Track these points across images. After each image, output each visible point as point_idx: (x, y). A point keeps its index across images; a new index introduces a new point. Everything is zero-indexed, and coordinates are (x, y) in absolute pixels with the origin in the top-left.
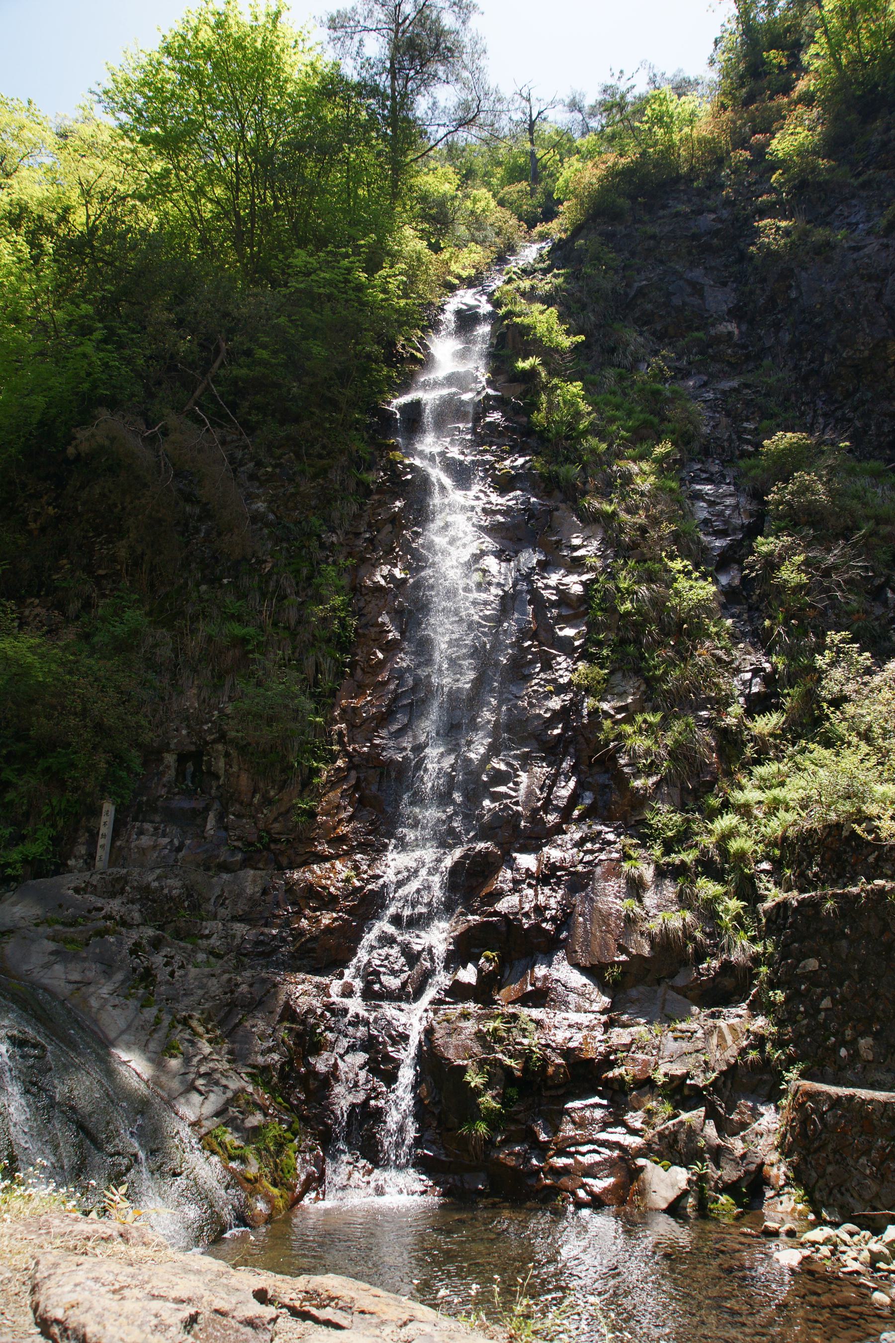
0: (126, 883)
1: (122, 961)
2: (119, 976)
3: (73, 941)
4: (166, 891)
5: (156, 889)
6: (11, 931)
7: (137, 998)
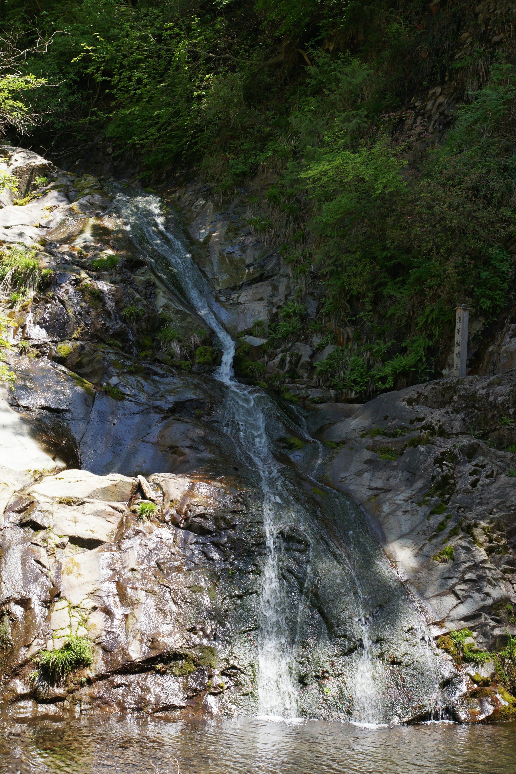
0: (455, 392)
1: (425, 470)
2: (419, 484)
3: (388, 451)
4: (491, 399)
5: (482, 397)
6: (343, 443)
7: (429, 505)
